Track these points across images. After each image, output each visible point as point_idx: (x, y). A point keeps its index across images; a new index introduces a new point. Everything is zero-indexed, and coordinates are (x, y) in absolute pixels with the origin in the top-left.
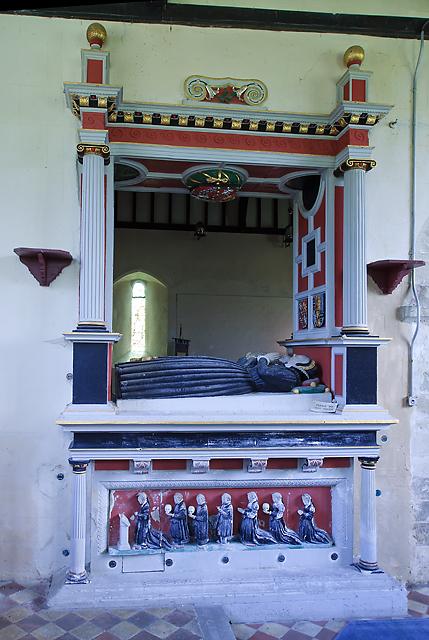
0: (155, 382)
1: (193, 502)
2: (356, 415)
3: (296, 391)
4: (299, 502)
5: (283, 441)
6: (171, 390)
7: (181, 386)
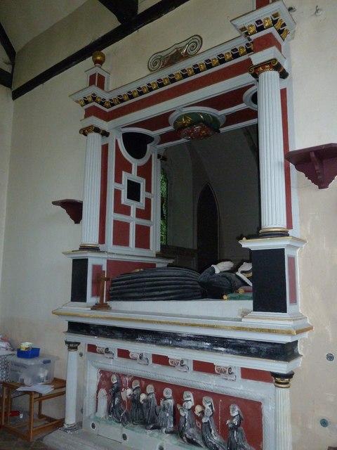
0: (128, 288)
1: (144, 391)
2: (269, 326)
3: (225, 297)
4: (226, 414)
5: (193, 344)
6: (136, 295)
7: (143, 292)
